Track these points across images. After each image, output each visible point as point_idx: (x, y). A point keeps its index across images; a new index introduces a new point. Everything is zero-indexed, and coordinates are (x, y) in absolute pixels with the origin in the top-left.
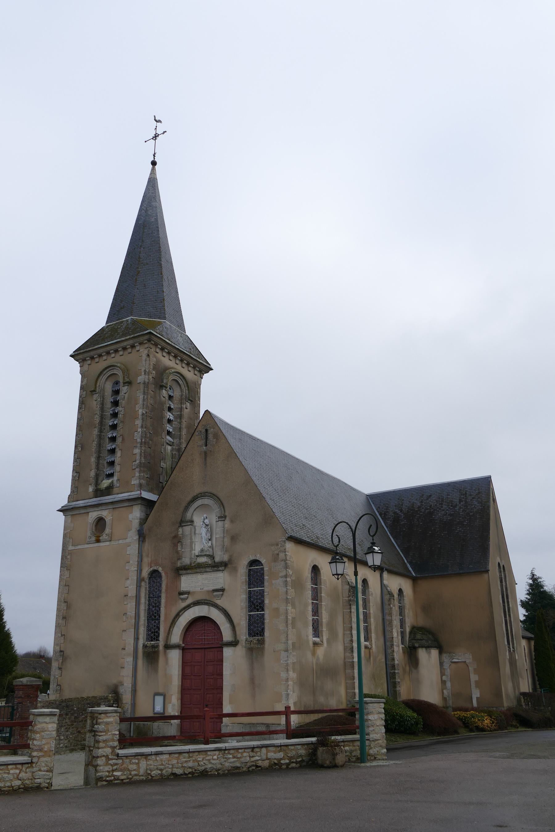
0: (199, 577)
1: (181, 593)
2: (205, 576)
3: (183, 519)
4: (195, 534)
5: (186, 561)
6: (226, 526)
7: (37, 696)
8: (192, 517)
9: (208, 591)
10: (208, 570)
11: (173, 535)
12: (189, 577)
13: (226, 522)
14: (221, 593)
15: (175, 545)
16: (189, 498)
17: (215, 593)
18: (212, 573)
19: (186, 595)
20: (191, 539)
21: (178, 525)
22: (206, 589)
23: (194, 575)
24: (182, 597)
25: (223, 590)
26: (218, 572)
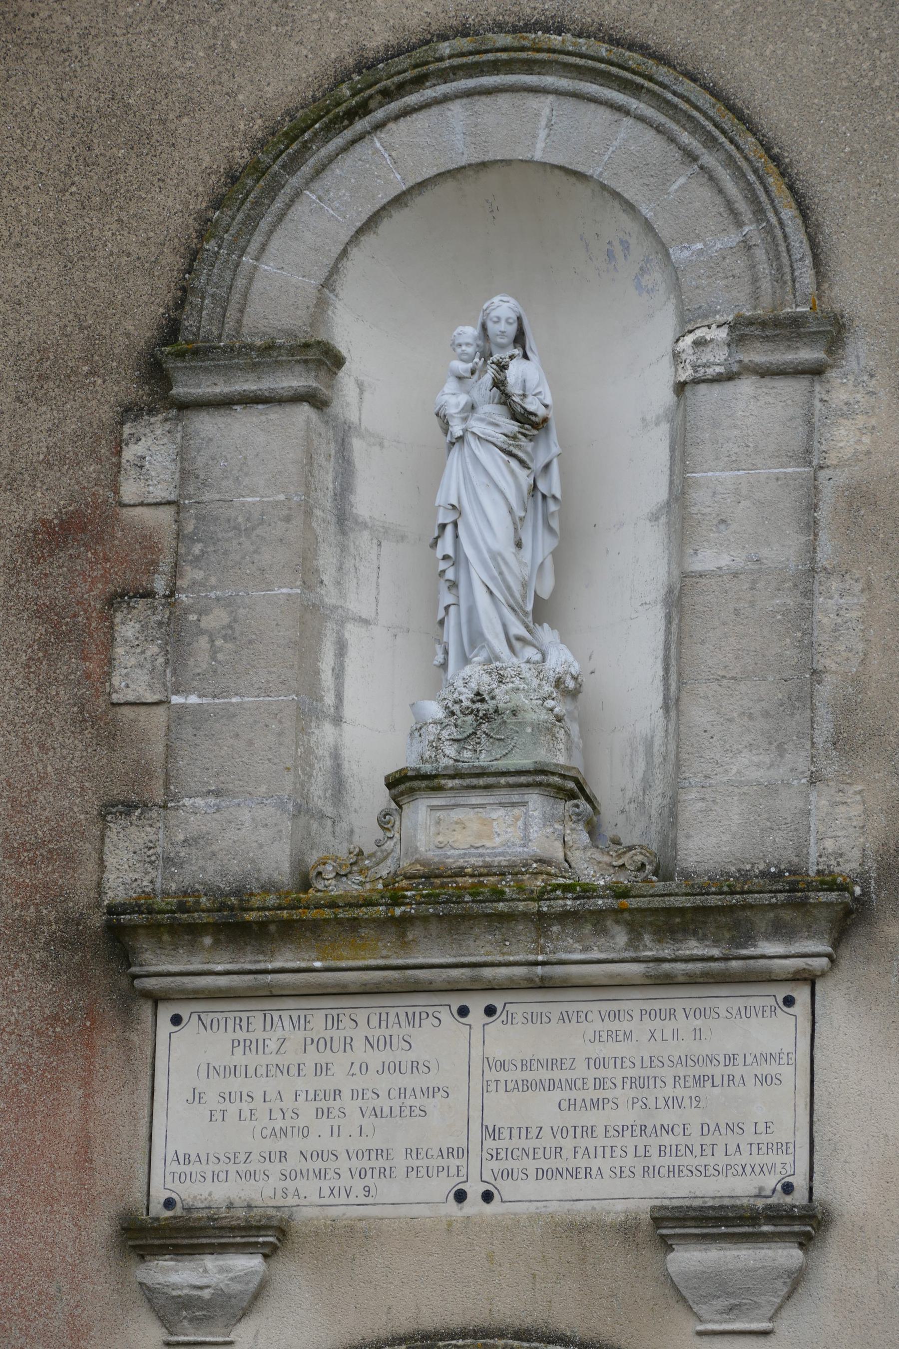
0: (442, 1042)
1: (149, 1236)
2: (522, 1033)
3: (199, 322)
4: (343, 519)
5: (240, 836)
6: (844, 439)
7: (734, 319)
8: (322, 304)
9: (576, 1232)
10: (575, 952)
11: (46, 502)
12: (286, 1034)
13: (840, 390)
14: (788, 1256)
15: (73, 637)
16: (287, 76)
17: (689, 1259)
18: (632, 1004)
19: (248, 1264)
20: (308, 574)
21: (121, 386)
22: (530, 1195)
23: (362, 1021)
24: (178, 1275)
25: (801, 1222)
26: (725, 1002)
